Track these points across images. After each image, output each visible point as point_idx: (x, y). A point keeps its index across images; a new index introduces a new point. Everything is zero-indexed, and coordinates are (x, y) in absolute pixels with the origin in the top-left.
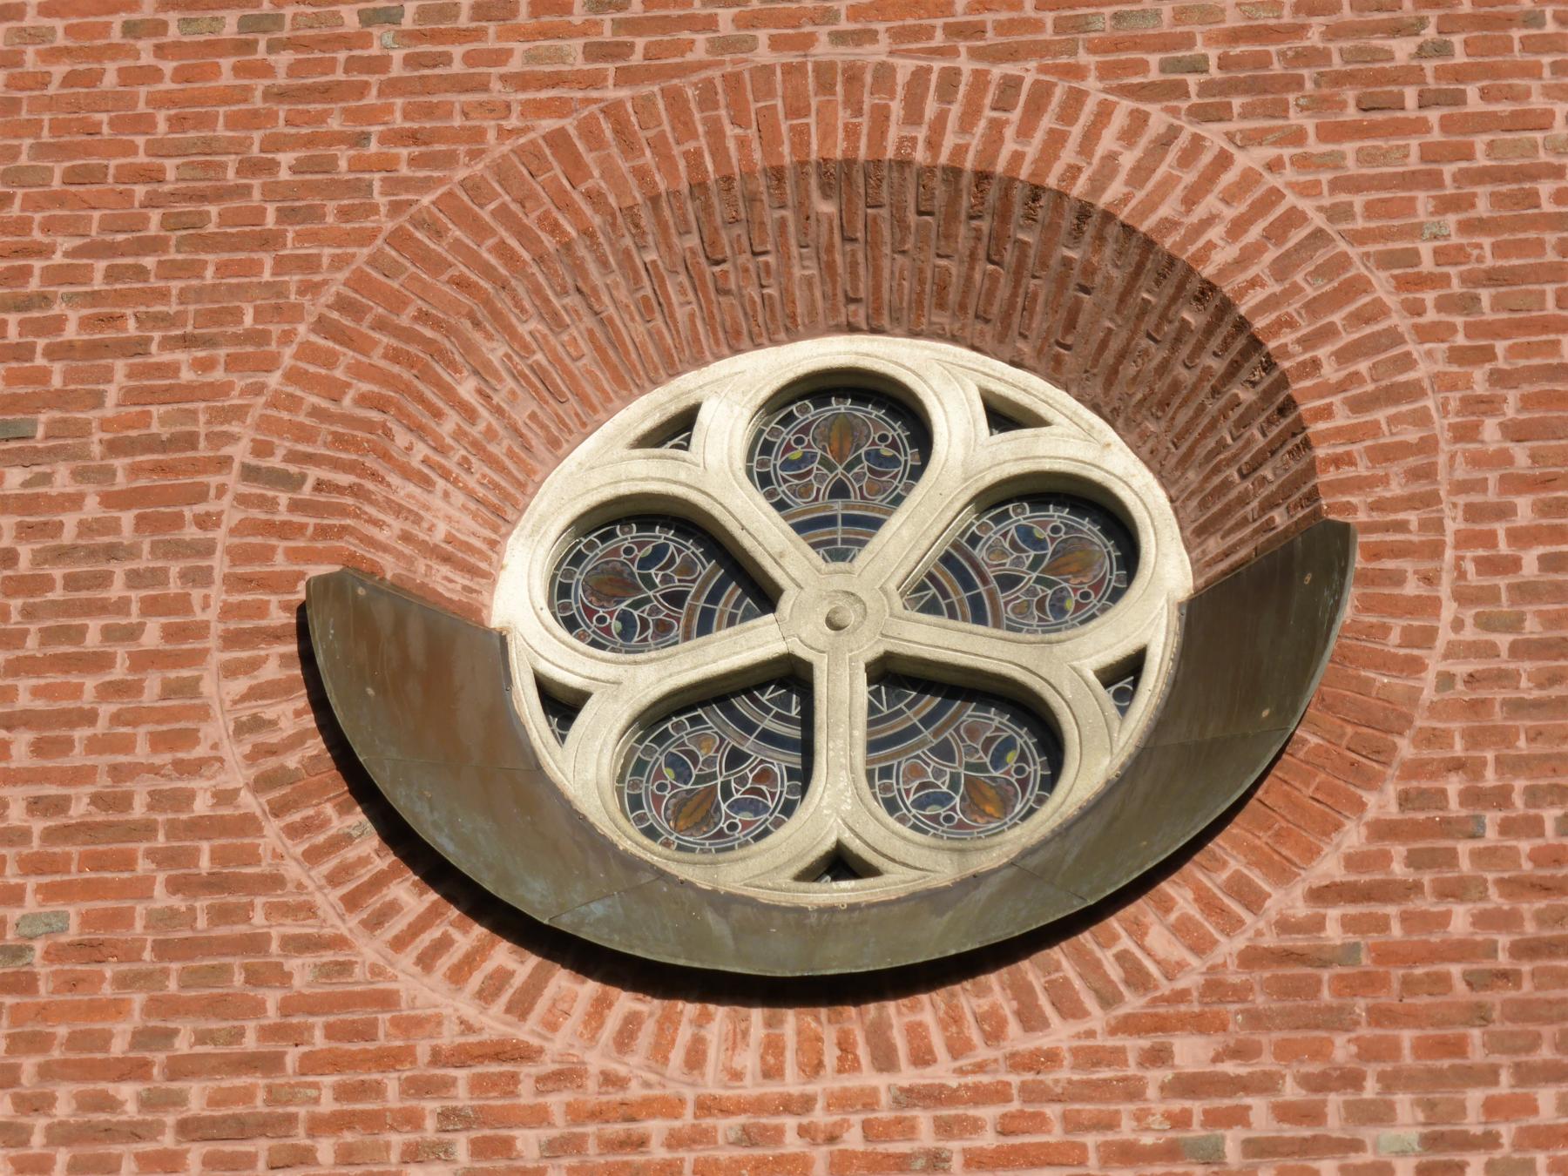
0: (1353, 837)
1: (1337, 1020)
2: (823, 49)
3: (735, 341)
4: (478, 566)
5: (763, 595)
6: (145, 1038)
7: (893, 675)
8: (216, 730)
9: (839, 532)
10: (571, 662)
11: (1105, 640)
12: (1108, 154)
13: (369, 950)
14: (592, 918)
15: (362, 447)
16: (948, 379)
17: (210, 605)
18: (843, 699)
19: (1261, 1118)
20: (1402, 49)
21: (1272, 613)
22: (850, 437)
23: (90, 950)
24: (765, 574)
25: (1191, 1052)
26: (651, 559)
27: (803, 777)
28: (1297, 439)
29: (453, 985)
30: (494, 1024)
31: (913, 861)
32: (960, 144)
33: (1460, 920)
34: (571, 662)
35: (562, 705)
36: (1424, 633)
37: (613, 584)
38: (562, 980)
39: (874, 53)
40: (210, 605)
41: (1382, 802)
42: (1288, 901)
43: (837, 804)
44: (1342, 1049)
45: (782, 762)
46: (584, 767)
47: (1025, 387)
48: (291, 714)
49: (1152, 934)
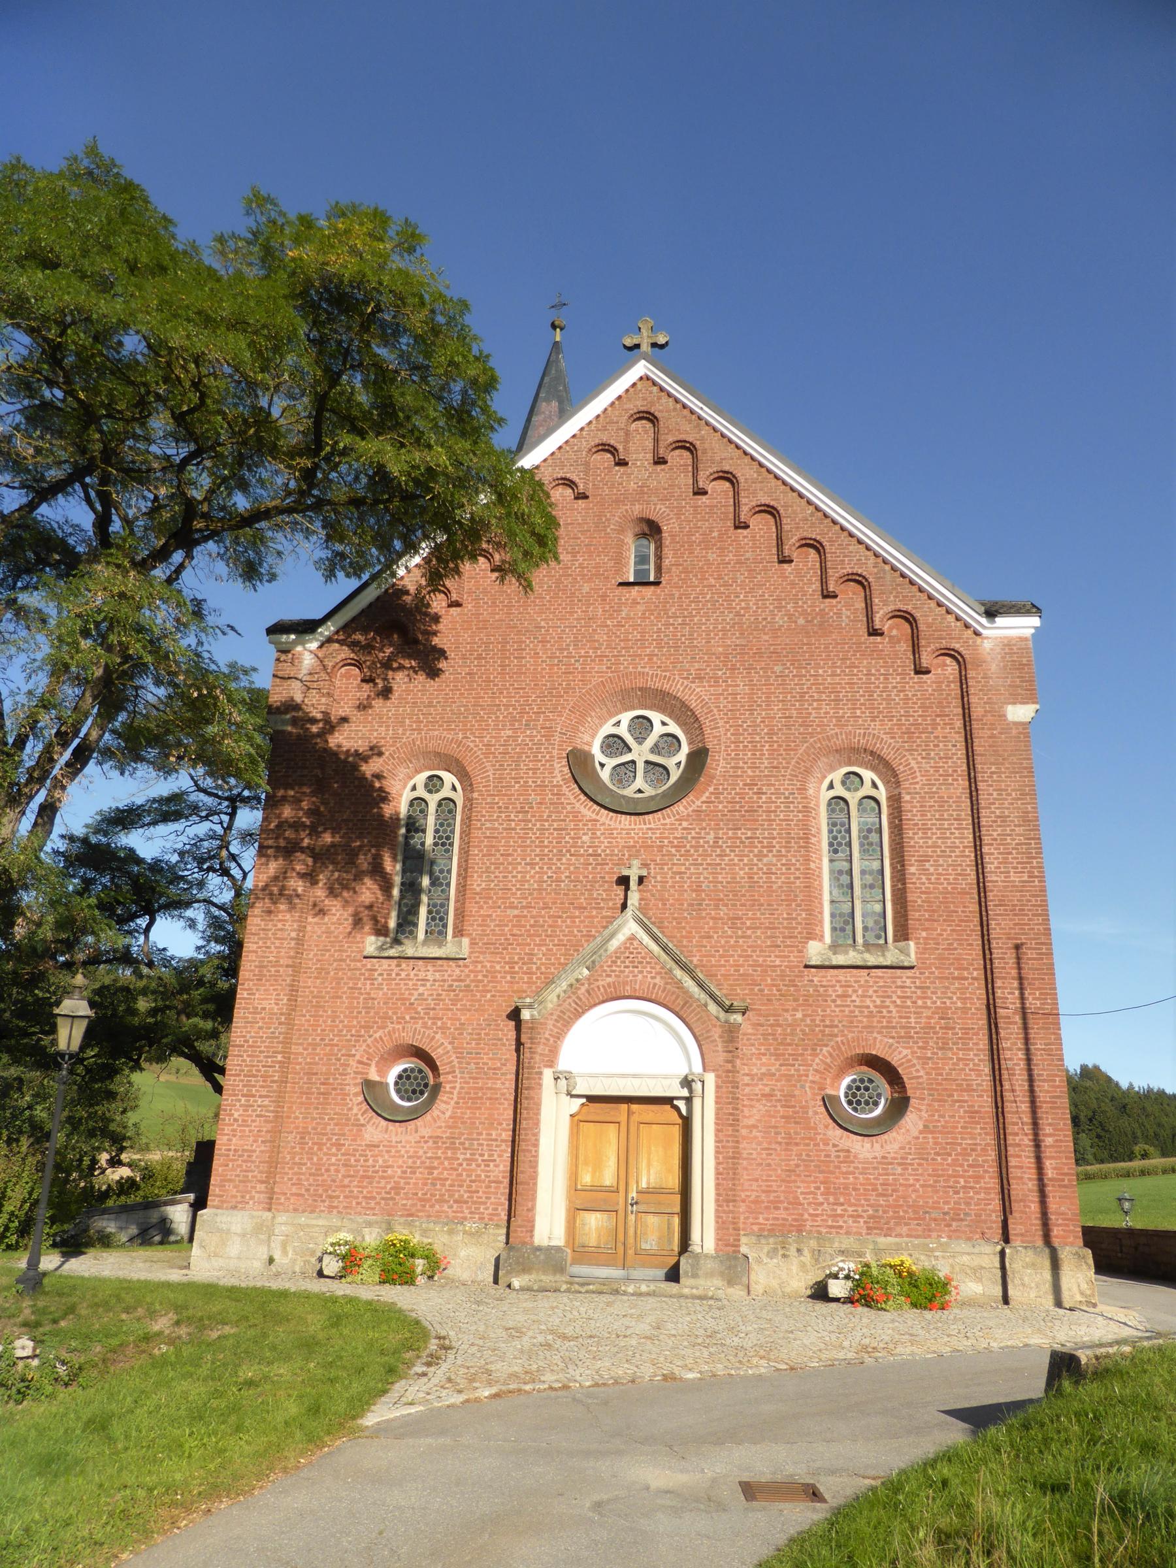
0: (707, 794)
1: (703, 820)
2: (639, 669)
3: (626, 710)
4: (590, 744)
5: (630, 750)
6: (549, 816)
7: (647, 762)
8: (556, 771)
9: (640, 740)
10: (604, 760)
11: (676, 759)
12: (678, 687)
13: (577, 805)
14: (607, 801)
15: (576, 730)
16: (656, 717)
17: (555, 752)
18: (640, 766)
19: (439, 1023)
20: (720, 673)
21: (698, 759)
22: (642, 725)
23: (541, 803)
24: (604, 389)
25: (685, 824)
26: (615, 744)
27: (635, 777)
28: (702, 734)
29: (588, 811)
30: (594, 816)
31: (649, 792)
32: (658, 685)
33: (720, 807)
34: (604, 760)
35: (602, 765)
36: (718, 765)
37: (609, 746)
38: (603, 810)
39: (647, 670)
40: (555, 752)
41: (711, 789)
42: (698, 803)
43: (639, 782)
44: (704, 824)
45: (632, 775)
46: (605, 775)
47: (667, 720)
48: (566, 770)
49: (680, 808)
